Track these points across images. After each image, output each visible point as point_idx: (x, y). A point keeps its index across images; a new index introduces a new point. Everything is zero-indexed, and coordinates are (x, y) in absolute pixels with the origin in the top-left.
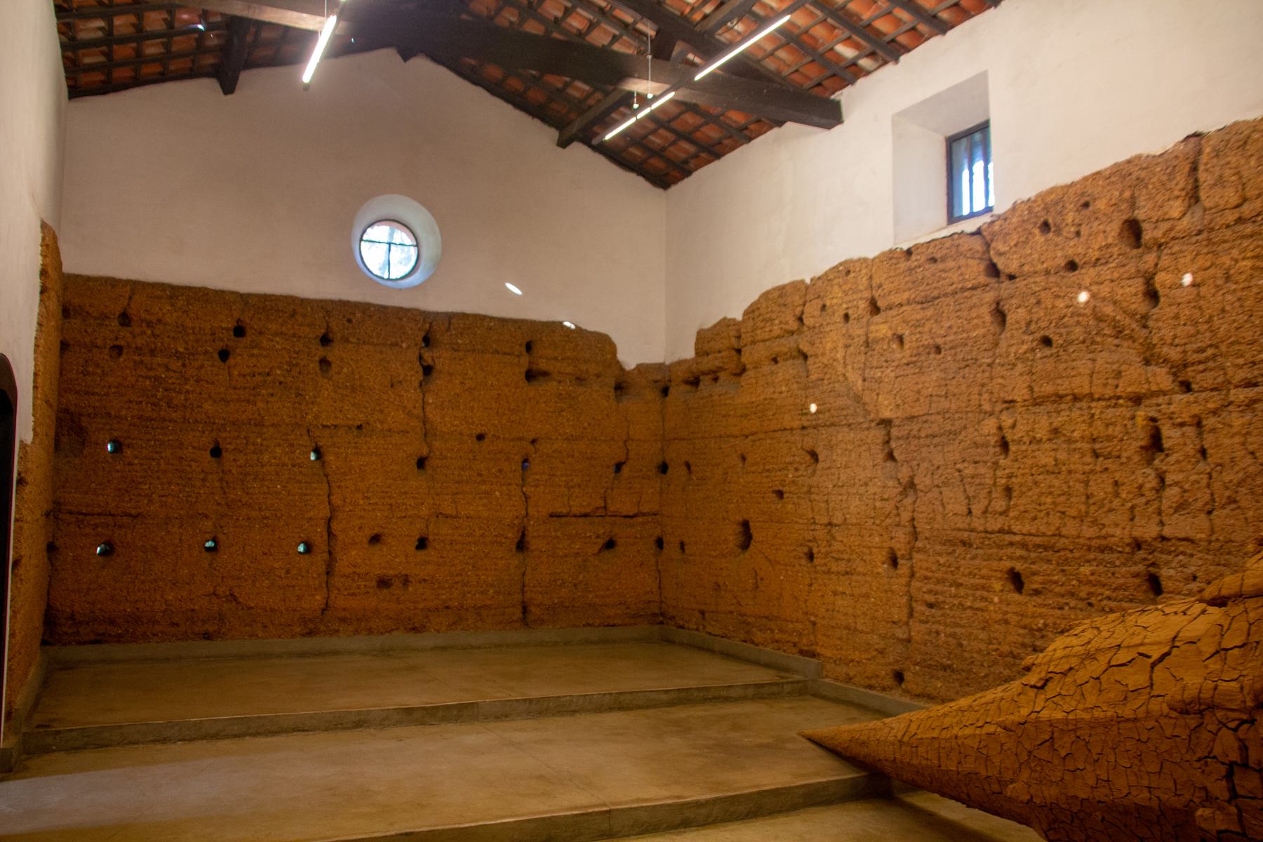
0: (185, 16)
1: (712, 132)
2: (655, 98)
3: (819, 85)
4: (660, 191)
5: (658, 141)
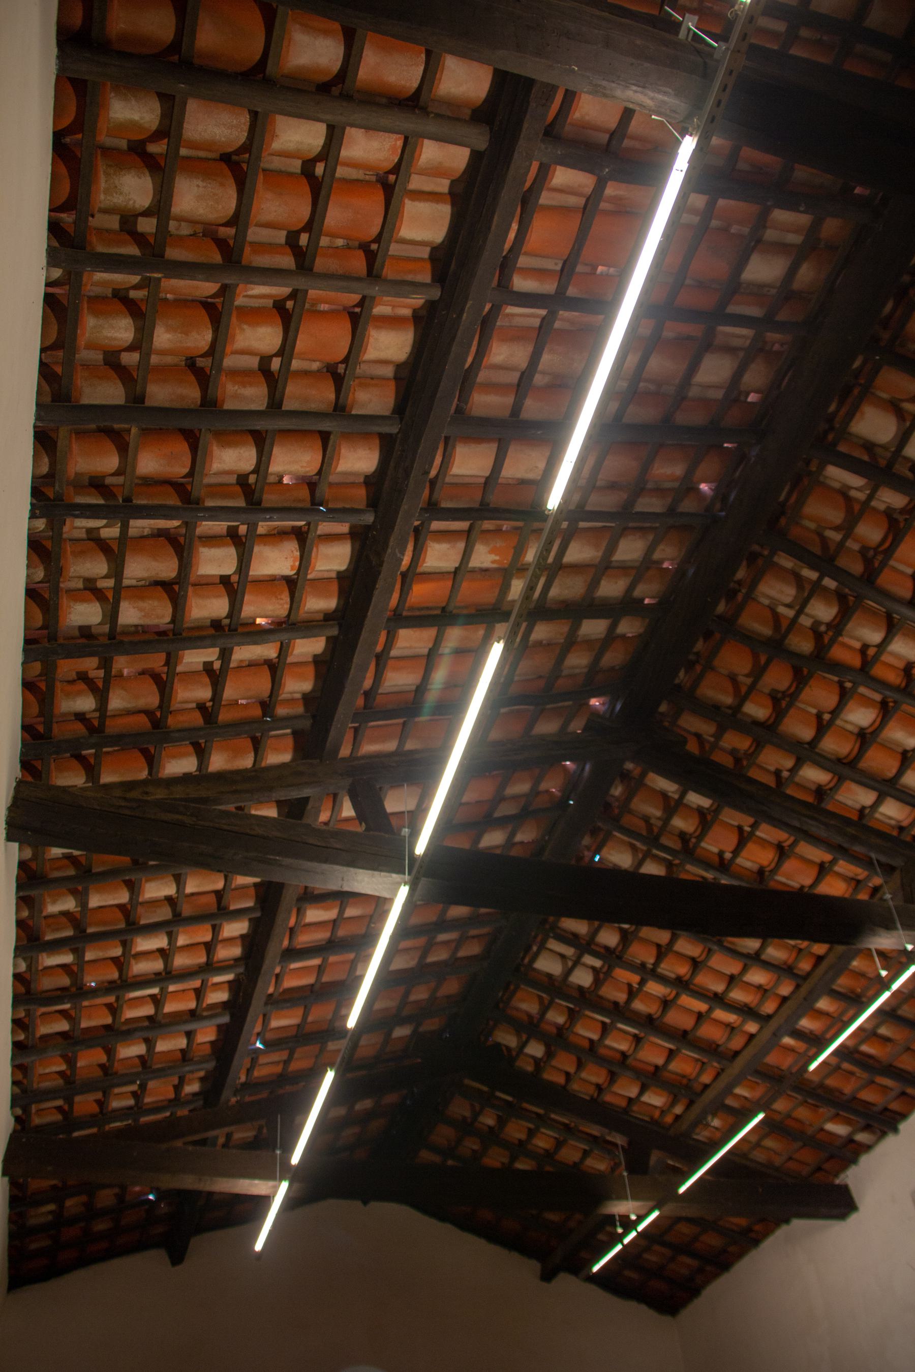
0: (137, 1189)
1: (712, 1240)
2: (641, 1218)
3: (819, 1169)
4: (668, 1319)
5: (654, 1258)
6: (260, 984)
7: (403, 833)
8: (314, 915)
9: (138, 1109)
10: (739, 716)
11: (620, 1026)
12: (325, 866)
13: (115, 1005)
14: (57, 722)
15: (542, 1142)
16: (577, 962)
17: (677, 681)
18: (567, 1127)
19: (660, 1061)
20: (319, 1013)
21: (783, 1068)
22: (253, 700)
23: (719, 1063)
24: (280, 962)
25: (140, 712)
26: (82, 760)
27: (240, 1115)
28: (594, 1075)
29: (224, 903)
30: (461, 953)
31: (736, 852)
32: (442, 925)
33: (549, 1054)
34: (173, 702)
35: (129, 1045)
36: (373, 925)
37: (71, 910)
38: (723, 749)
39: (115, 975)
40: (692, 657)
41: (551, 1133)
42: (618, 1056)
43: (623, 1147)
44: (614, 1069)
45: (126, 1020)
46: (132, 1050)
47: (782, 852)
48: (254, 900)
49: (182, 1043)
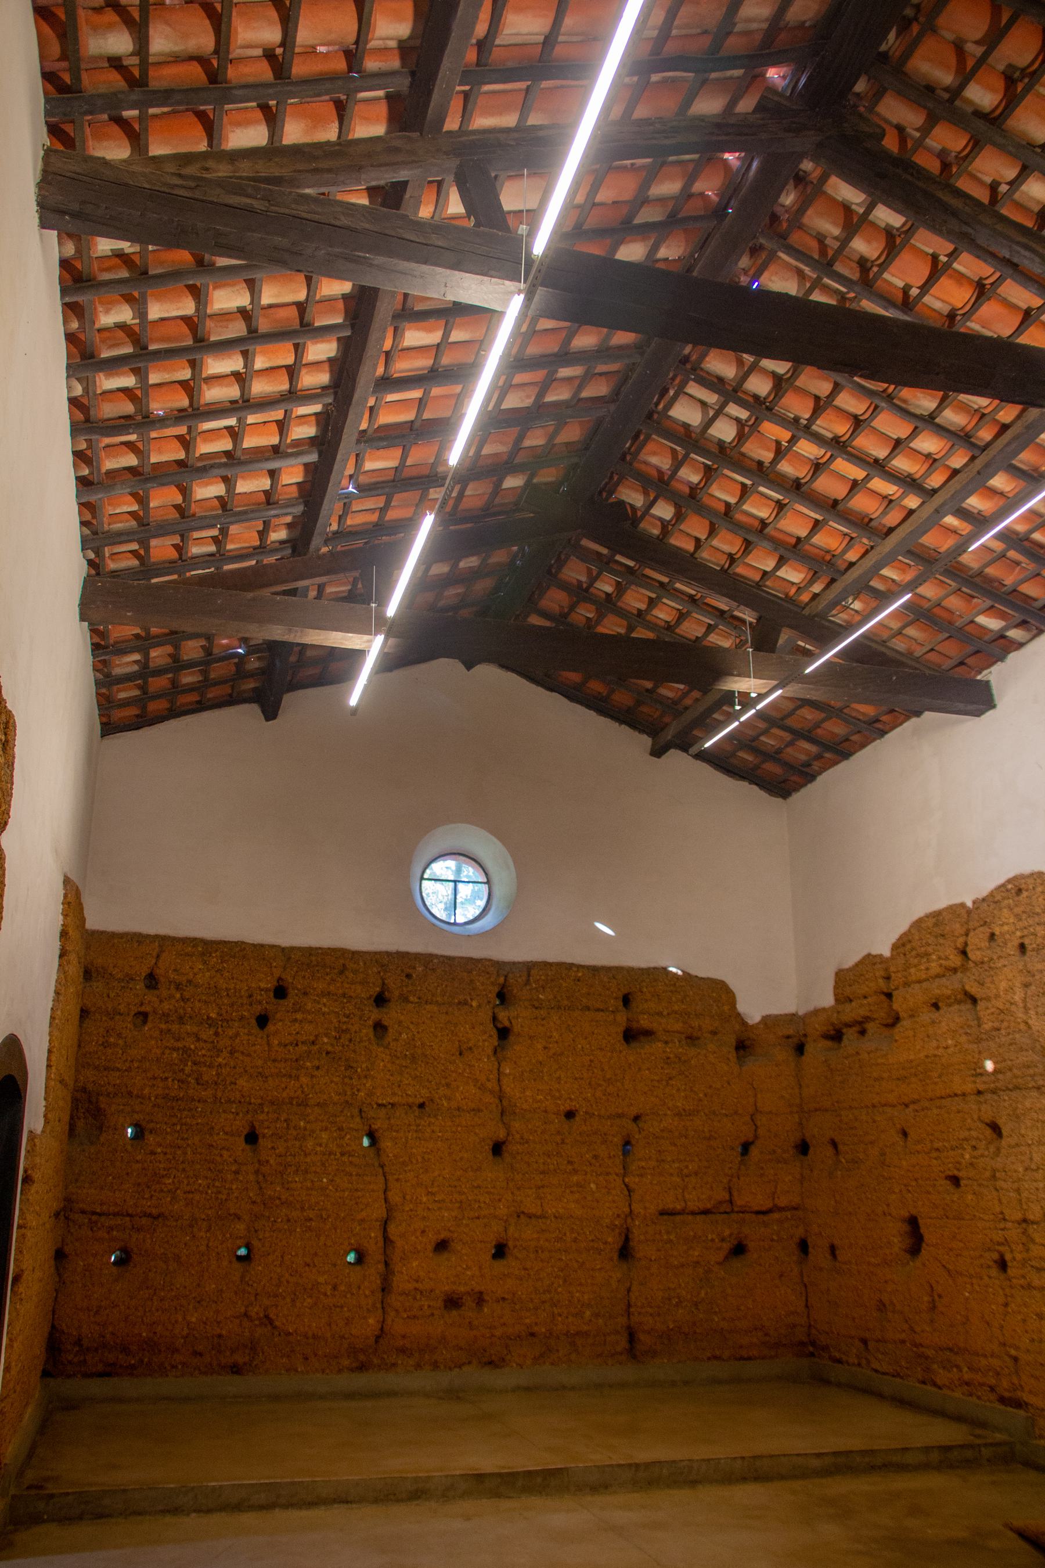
1: (836, 728)
2: (761, 697)
6: (351, 416)
7: (519, 232)
8: (414, 337)
9: (220, 556)
10: (957, 103)
11: (762, 489)
12: (425, 268)
13: (188, 438)
14: (86, 70)
15: (663, 614)
16: (719, 412)
17: (883, 48)
18: (692, 598)
19: (803, 533)
20: (419, 455)
21: (941, 550)
22: (336, 47)
23: (869, 539)
24: (374, 392)
25: (192, 58)
26: (123, 124)
27: (333, 565)
28: (727, 543)
29: (307, 319)
30: (584, 394)
31: (925, 288)
32: (565, 357)
33: (679, 517)
34: (232, 47)
35: (207, 484)
36: (483, 353)
37: (129, 322)
38: (929, 150)
39: (185, 402)
40: (909, 12)
41: (673, 604)
42: (756, 524)
43: (751, 624)
44: (750, 538)
45: (201, 455)
46: (208, 491)
47: (982, 291)
48: (343, 315)
49: (266, 483)
